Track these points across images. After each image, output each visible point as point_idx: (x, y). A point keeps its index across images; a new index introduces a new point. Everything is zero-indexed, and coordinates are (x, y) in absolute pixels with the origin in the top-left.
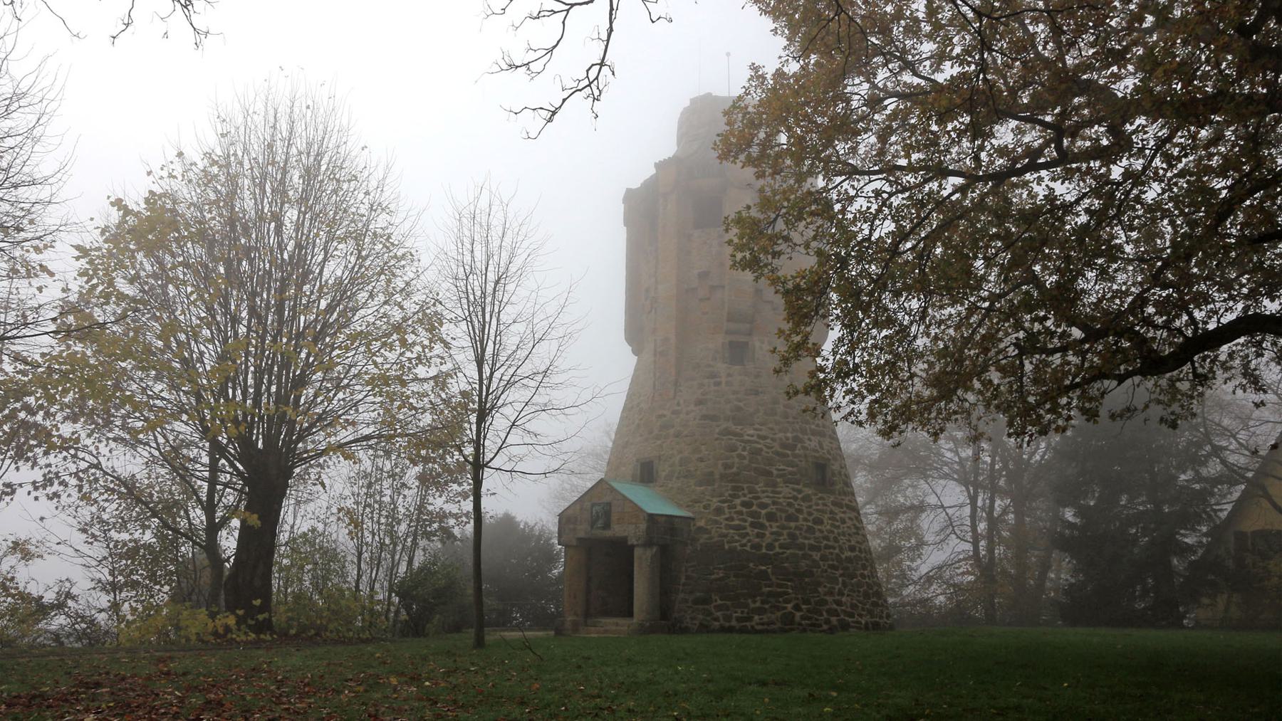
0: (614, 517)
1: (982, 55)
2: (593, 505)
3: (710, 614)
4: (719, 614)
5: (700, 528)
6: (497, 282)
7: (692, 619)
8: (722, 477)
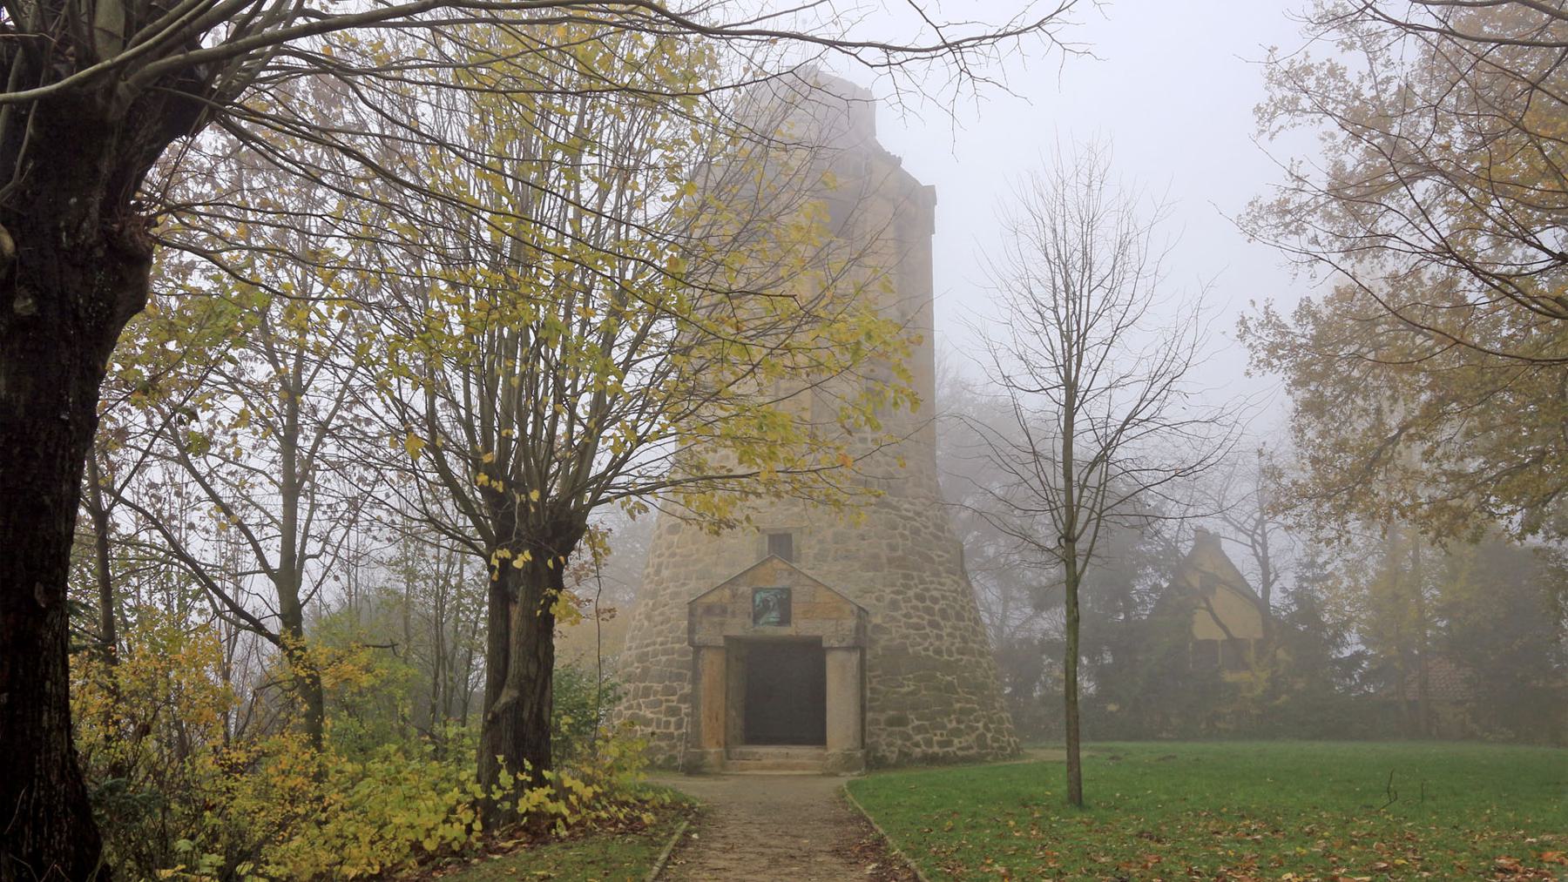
0: (796, 609)
1: (453, 177)
2: (756, 591)
3: (909, 738)
4: (918, 738)
5: (877, 626)
6: (1123, 246)
7: (890, 745)
8: (890, 561)
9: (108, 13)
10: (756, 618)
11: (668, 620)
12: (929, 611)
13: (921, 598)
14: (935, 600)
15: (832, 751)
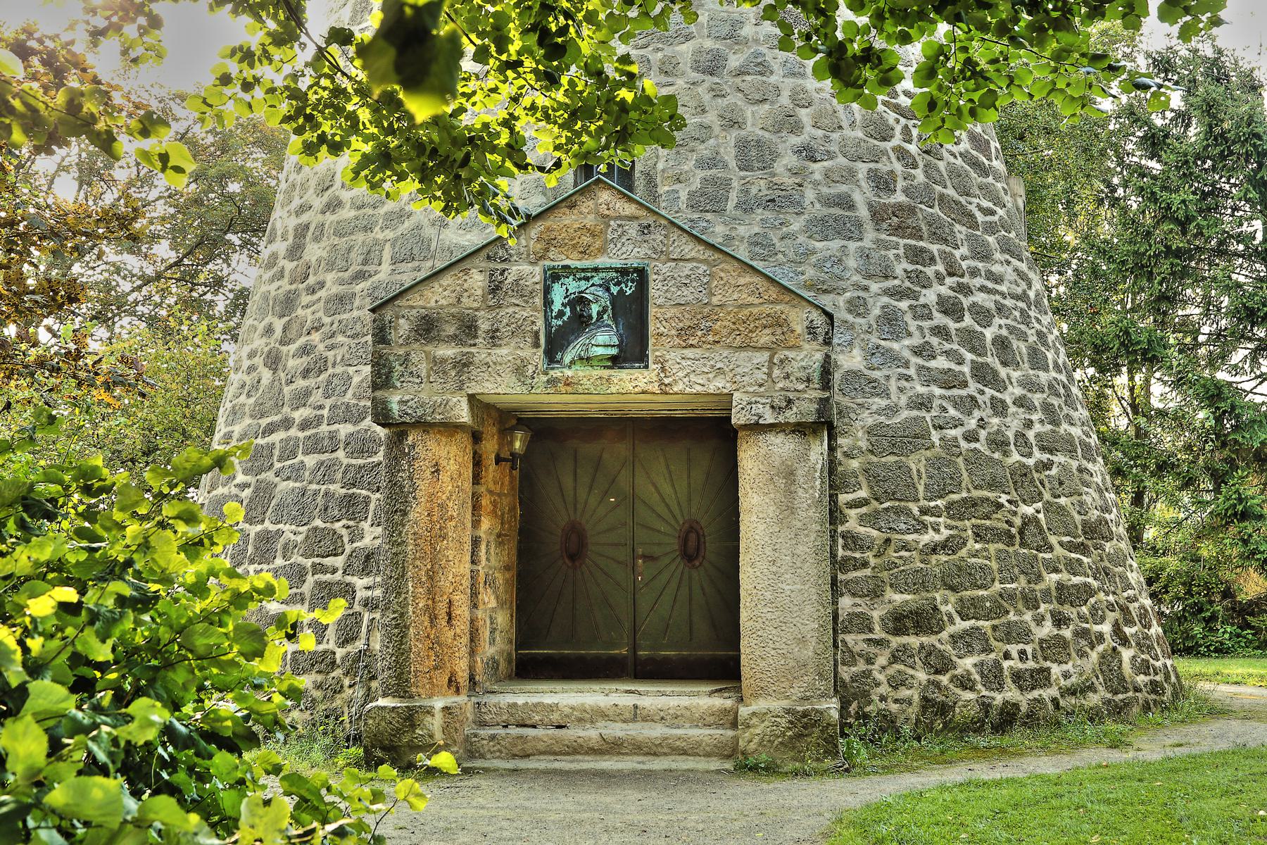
2: (554, 276)
3: (941, 664)
9: (3, 214)
10: (554, 346)
11: (320, 366)
12: (972, 341)
13: (950, 308)
14: (983, 316)
15: (760, 705)
